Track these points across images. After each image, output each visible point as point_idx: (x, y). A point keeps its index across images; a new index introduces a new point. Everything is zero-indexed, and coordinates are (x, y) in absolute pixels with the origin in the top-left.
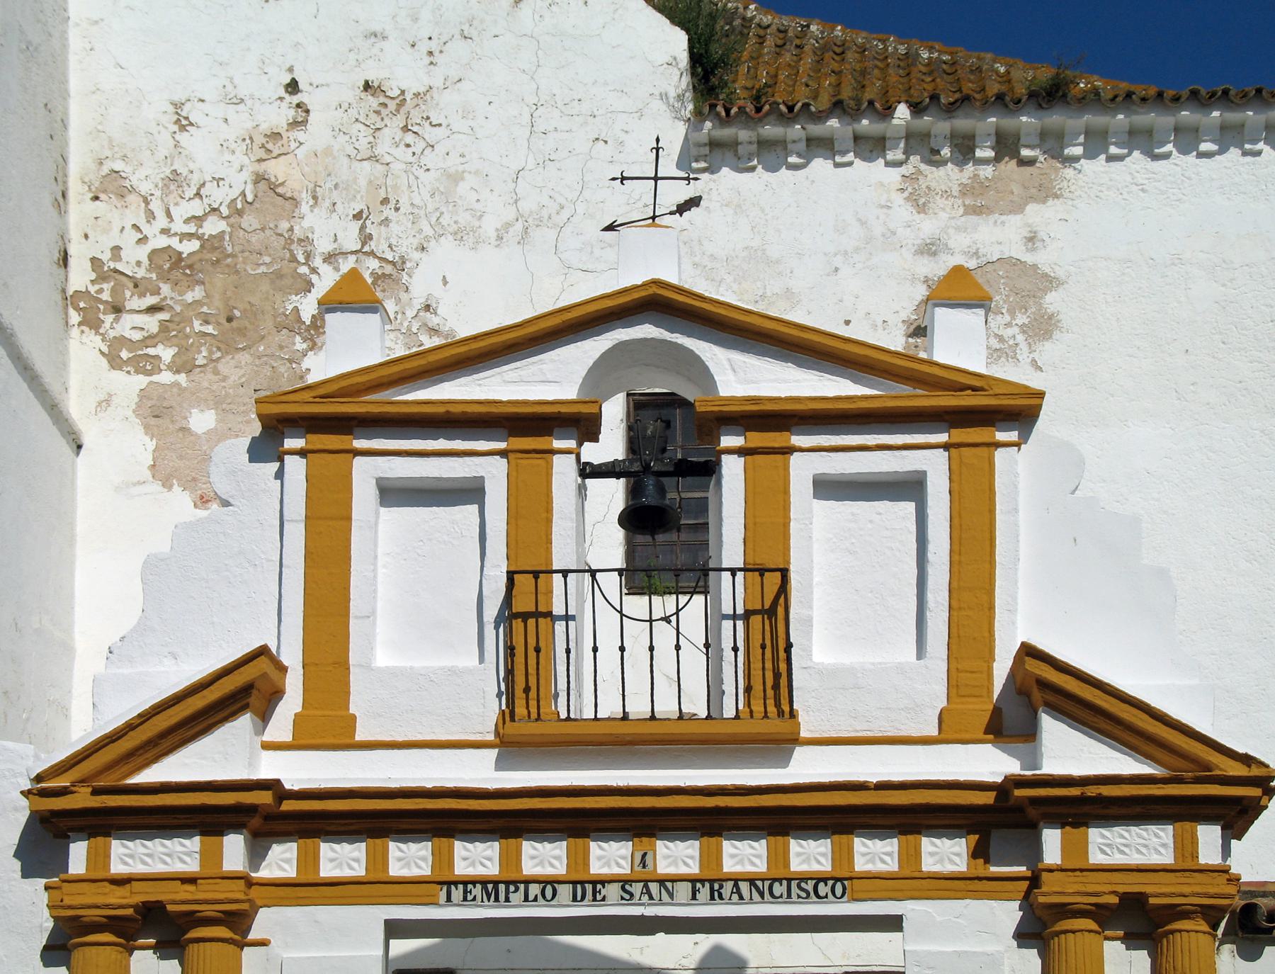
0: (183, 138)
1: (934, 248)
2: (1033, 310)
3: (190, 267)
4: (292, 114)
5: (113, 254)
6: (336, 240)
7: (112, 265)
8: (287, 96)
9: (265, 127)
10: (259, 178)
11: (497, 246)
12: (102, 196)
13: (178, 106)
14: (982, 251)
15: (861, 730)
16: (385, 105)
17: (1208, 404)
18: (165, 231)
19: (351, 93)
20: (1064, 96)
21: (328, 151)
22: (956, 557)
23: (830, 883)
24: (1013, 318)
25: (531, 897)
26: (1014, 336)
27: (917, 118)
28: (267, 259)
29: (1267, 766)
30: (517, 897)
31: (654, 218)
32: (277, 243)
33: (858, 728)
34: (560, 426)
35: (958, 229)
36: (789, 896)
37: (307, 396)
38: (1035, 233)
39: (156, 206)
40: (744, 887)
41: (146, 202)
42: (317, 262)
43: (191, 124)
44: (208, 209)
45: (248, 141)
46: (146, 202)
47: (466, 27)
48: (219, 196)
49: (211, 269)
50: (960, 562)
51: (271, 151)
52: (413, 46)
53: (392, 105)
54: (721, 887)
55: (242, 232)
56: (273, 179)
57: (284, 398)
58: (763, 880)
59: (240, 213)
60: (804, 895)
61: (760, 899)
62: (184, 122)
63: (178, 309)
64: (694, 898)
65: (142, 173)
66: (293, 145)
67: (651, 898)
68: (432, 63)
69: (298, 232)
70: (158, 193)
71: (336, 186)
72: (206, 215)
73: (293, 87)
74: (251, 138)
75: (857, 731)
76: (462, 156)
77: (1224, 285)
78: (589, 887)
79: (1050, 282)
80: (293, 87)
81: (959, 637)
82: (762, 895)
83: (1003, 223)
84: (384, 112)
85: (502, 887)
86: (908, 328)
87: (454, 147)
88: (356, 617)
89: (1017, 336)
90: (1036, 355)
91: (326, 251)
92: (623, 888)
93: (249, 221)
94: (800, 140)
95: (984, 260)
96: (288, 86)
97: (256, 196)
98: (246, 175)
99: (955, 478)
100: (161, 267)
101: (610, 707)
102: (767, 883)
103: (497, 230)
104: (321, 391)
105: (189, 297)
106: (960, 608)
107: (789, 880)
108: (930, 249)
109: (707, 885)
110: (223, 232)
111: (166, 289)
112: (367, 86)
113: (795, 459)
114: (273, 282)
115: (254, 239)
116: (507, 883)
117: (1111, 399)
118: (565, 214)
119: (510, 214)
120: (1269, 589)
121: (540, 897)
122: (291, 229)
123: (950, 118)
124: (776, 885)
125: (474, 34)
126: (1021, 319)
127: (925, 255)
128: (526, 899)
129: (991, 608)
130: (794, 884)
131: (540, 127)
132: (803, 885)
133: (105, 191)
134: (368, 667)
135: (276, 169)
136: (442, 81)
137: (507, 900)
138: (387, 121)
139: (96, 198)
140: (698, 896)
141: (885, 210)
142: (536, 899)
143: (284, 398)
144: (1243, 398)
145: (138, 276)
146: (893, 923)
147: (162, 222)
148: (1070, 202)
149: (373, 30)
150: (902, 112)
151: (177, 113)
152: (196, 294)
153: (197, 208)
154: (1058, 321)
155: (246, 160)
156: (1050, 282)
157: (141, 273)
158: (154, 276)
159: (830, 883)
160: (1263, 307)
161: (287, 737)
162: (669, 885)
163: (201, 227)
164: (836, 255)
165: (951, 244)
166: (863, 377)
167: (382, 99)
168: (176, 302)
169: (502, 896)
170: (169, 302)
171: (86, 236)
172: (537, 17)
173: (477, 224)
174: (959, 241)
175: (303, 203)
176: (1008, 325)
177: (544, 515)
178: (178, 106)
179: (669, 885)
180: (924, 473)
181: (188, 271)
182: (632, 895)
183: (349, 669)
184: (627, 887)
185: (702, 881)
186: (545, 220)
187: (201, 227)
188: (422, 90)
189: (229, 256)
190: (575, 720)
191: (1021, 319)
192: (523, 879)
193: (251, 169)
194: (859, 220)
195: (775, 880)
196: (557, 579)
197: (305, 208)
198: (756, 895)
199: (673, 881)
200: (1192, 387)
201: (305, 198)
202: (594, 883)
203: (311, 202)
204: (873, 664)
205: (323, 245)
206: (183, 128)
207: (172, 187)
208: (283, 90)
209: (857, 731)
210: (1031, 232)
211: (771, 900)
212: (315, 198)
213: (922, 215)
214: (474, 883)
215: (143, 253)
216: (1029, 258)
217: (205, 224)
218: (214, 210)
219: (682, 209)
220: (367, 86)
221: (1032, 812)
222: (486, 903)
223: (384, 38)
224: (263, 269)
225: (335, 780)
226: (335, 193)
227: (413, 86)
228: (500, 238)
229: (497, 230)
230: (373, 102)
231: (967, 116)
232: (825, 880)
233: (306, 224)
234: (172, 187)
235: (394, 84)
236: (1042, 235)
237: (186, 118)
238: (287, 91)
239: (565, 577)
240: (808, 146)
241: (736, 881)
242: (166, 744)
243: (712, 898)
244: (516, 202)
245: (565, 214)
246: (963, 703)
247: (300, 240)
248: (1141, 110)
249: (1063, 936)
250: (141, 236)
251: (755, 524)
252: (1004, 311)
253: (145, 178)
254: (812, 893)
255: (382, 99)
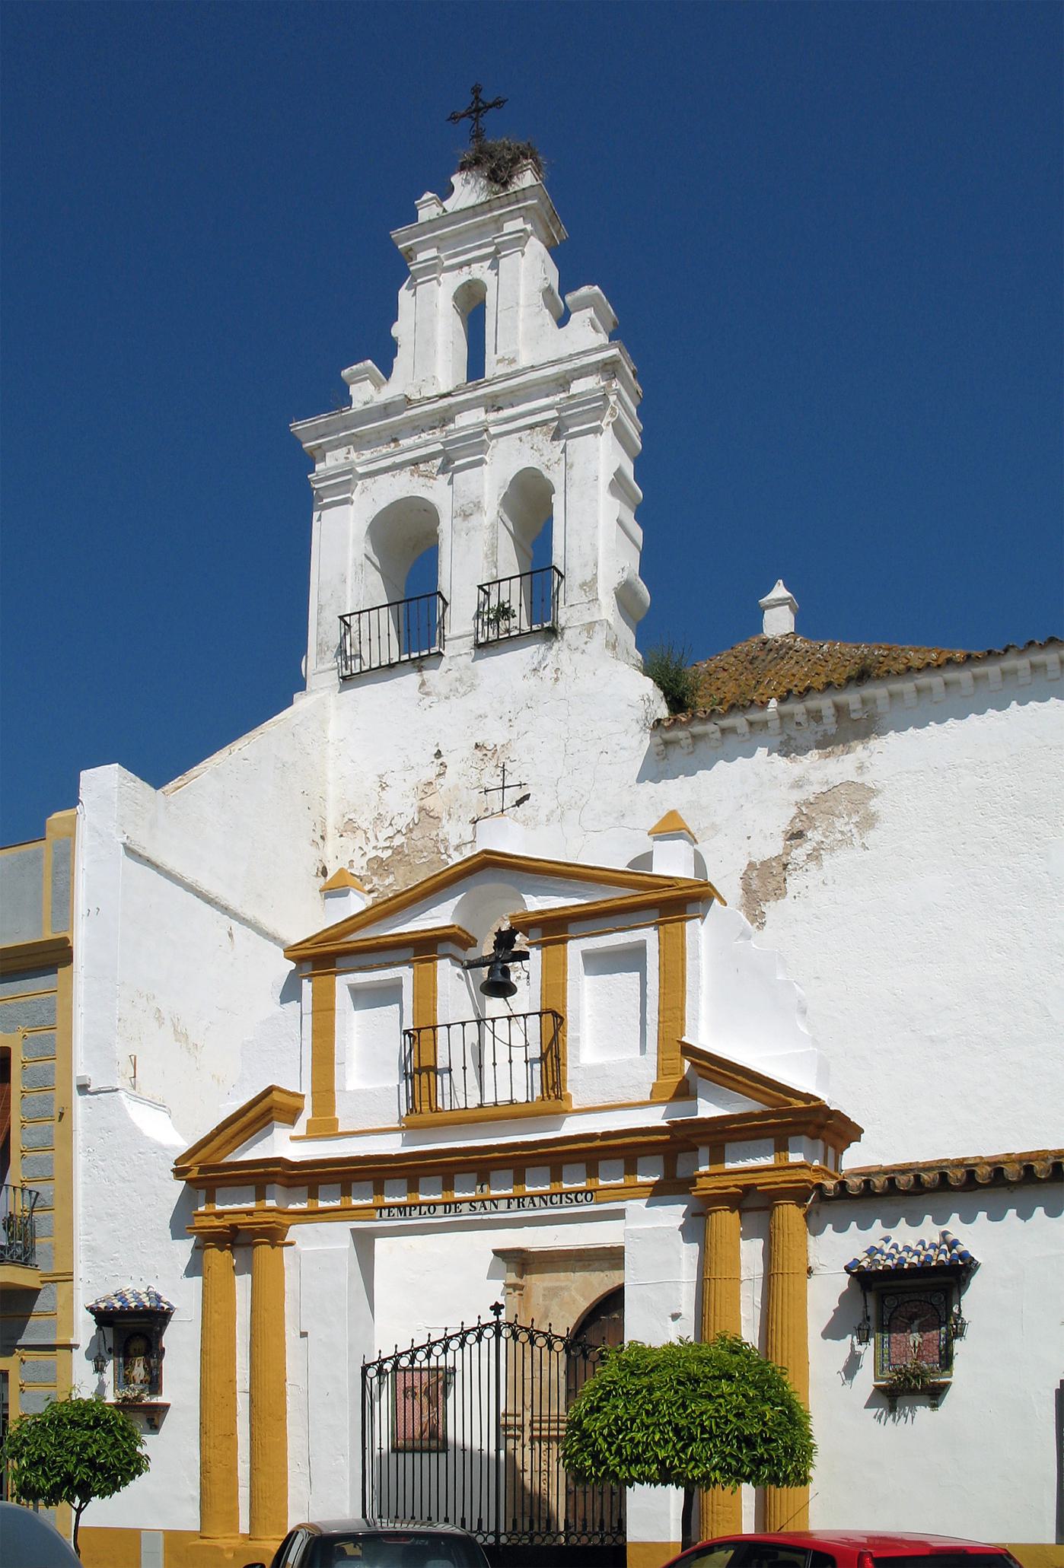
0: (383, 794)
1: (801, 783)
2: (863, 812)
3: (387, 865)
4: (437, 770)
5: (350, 865)
6: (460, 837)
7: (349, 871)
8: (436, 760)
9: (424, 780)
10: (421, 809)
11: (547, 825)
12: (344, 834)
13: (381, 776)
14: (830, 780)
15: (607, 1100)
16: (486, 755)
17: (973, 855)
18: (375, 848)
19: (467, 751)
20: (869, 676)
21: (456, 787)
22: (662, 990)
23: (584, 1194)
24: (850, 818)
25: (423, 1213)
26: (851, 831)
27: (781, 705)
28: (425, 854)
29: (820, 1099)
30: (415, 1213)
31: (503, 811)
32: (431, 844)
33: (606, 1100)
34: (441, 942)
35: (815, 768)
36: (561, 1203)
37: (307, 945)
38: (863, 763)
39: (370, 835)
40: (536, 1200)
41: (366, 833)
42: (451, 851)
43: (387, 786)
44: (396, 832)
45: (416, 789)
46: (366, 833)
47: (529, 702)
48: (401, 823)
49: (397, 864)
50: (664, 994)
51: (426, 793)
52: (501, 718)
53: (490, 754)
54: (524, 1200)
55: (413, 841)
56: (428, 808)
57: (300, 947)
58: (546, 1195)
59: (411, 831)
60: (570, 1201)
61: (545, 1206)
62: (384, 785)
63: (381, 889)
64: (509, 1207)
65: (363, 818)
66: (438, 787)
67: (485, 1209)
68: (511, 726)
69: (441, 836)
70: (371, 827)
71: (461, 806)
72: (395, 835)
73: (438, 754)
74: (417, 788)
75: (605, 1102)
76: (528, 776)
77: (982, 777)
78: (453, 1206)
79: (873, 792)
80: (438, 754)
81: (664, 1039)
82: (546, 1203)
83: (843, 760)
84: (486, 758)
85: (408, 1209)
86: (786, 835)
87: (523, 771)
88: (338, 1064)
89: (853, 830)
90: (863, 841)
91: (455, 844)
92: (471, 1205)
93: (416, 834)
94: (716, 731)
95: (832, 786)
96: (436, 754)
97: (419, 820)
98: (415, 809)
99: (662, 942)
100: (373, 868)
101: (504, 1096)
102: (549, 1197)
103: (547, 816)
104: (315, 941)
105: (387, 883)
106: (664, 1022)
107: (561, 1194)
108: (798, 784)
109: (516, 1200)
110: (403, 843)
111: (375, 879)
112: (477, 746)
113: (570, 943)
114: (428, 866)
115: (419, 843)
116: (410, 1206)
117: (912, 861)
118: (584, 800)
119: (554, 804)
120: (1012, 969)
121: (427, 1212)
122: (438, 835)
123: (802, 702)
124: (554, 1196)
125: (533, 705)
126: (855, 819)
127: (796, 789)
128: (420, 1214)
129: (683, 1019)
130: (564, 1196)
131: (570, 751)
132: (569, 1196)
133: (346, 831)
134: (344, 1091)
135: (429, 803)
136: (516, 734)
137: (410, 1215)
138: (487, 764)
139: (341, 836)
140: (511, 1206)
141: (770, 765)
142: (425, 1214)
143: (300, 947)
144: (995, 848)
145: (362, 875)
146: (619, 1215)
147: (373, 843)
148: (884, 741)
149: (479, 714)
150: (773, 703)
151: (381, 781)
152: (390, 880)
153: (390, 832)
154: (878, 817)
155: (414, 800)
156: (873, 792)
157: (363, 873)
158: (369, 873)
159: (584, 1194)
160: (1007, 788)
161: (304, 1133)
162: (496, 1202)
163: (392, 842)
164: (741, 797)
165: (812, 778)
166: (621, 890)
167: (485, 752)
168: (381, 886)
169: (408, 1213)
170: (377, 886)
171: (337, 857)
172: (567, 687)
173: (536, 813)
174: (816, 776)
175: (444, 819)
176: (847, 824)
177: (432, 995)
178: (381, 776)
179: (496, 1202)
180: (645, 941)
181: (386, 868)
182: (475, 1208)
183: (334, 1093)
184: (473, 1204)
185: (514, 1198)
186: (573, 805)
187: (392, 842)
188: (505, 742)
189: (406, 856)
190: (457, 1110)
191: (855, 819)
192: (490, 1197)
193: (417, 805)
194: (755, 773)
195: (553, 1194)
196: (489, 1023)
197: (444, 821)
198: (543, 1205)
199: (498, 1199)
200: (962, 846)
201: (444, 816)
202: (455, 1203)
203: (448, 817)
204: (615, 1061)
205: (454, 841)
206: (383, 789)
207: (378, 822)
208: (433, 757)
209: (605, 1102)
210: (860, 763)
211: (430, 1215)
212: (450, 815)
213: (793, 764)
214: (393, 1207)
215: (363, 862)
216: (859, 780)
217: (395, 840)
218: (399, 831)
219: (519, 803)
220: (477, 746)
221: (694, 1140)
222: (400, 1217)
223: (486, 717)
224: (424, 860)
225: (316, 1155)
226: (460, 810)
227: (500, 741)
228: (548, 820)
229: (547, 816)
230: (479, 754)
231: (752, 714)
232: (581, 1192)
233: (445, 830)
234: (378, 822)
235: (490, 742)
236: (867, 764)
237: (385, 783)
238: (435, 757)
239: (525, 1018)
240: (722, 734)
241: (532, 1197)
242: (235, 1142)
243: (519, 1207)
244: (557, 797)
245: (584, 800)
246: (666, 1079)
247: (442, 840)
248: (919, 676)
249: (714, 1214)
250: (363, 852)
251: (546, 985)
252: (844, 816)
253: (364, 821)
254: (574, 1200)
255: (485, 752)
